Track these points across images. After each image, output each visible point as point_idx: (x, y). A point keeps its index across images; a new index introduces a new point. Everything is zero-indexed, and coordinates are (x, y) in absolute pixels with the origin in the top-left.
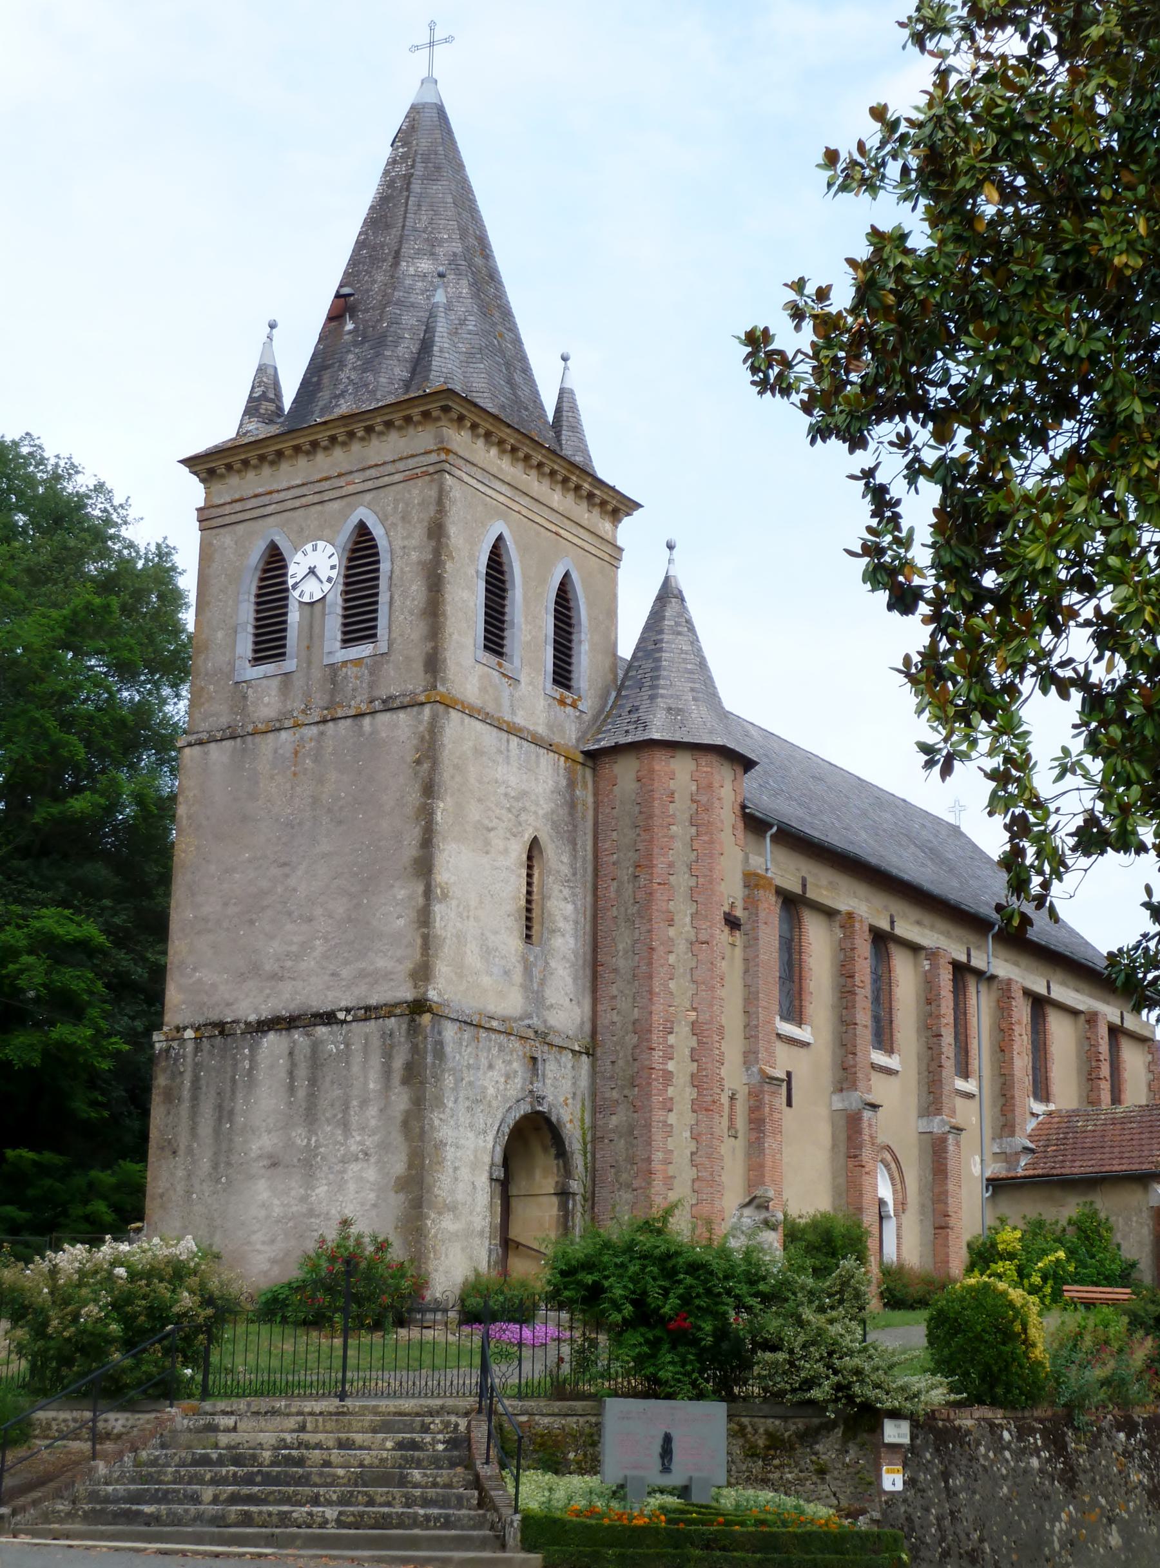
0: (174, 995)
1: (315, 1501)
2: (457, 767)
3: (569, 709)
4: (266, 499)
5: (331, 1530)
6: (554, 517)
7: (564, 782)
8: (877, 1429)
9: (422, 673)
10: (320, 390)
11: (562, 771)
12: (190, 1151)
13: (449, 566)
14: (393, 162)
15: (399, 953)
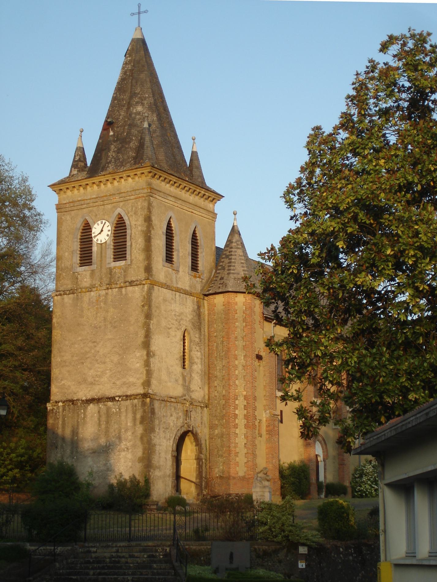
0: (54, 389)
1: (124, 574)
2: (157, 307)
3: (198, 279)
7: (196, 307)
9: (144, 273)
10: (101, 159)
11: (195, 303)
12: (62, 447)
13: (152, 232)
14: (125, 64)
15: (138, 376)
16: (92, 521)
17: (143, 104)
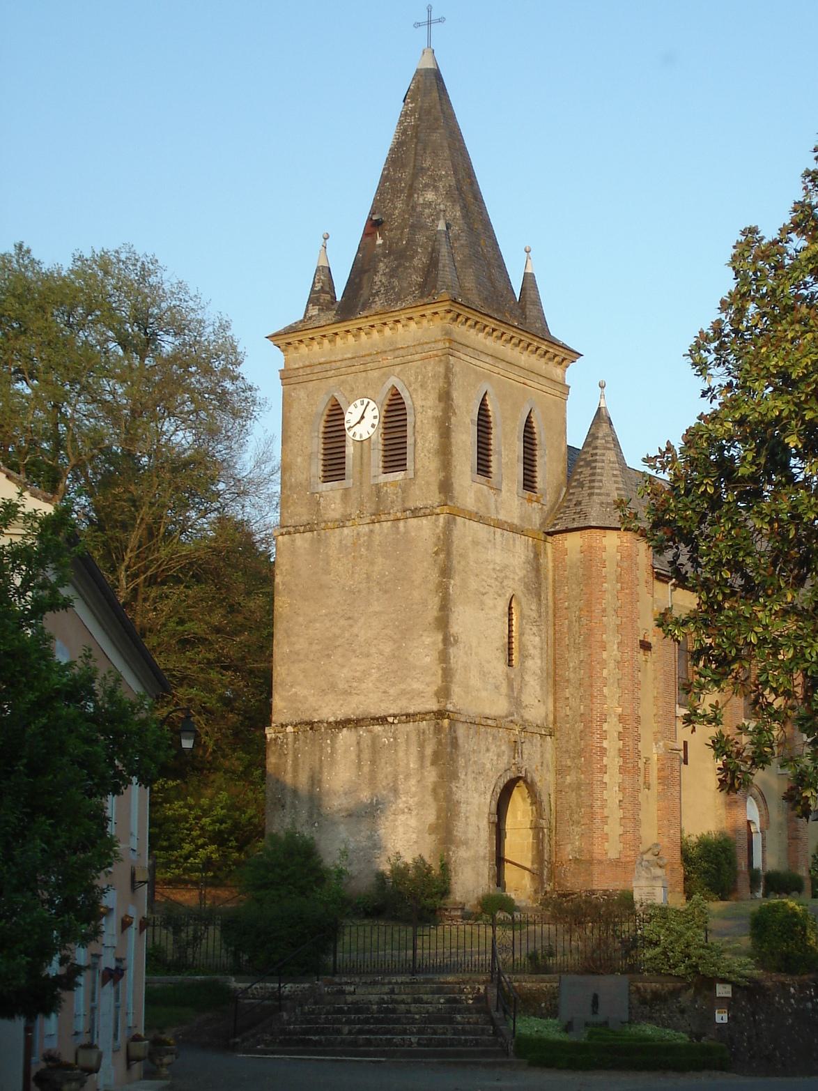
0: (278, 702)
1: (404, 1032)
2: (461, 555)
3: (535, 504)
4: (328, 366)
5: (415, 1047)
6: (522, 373)
7: (532, 555)
8: (713, 989)
10: (361, 289)
12: (294, 806)
13: (453, 419)
14: (405, 115)
15: (428, 679)
16: (347, 938)
17: (436, 189)
